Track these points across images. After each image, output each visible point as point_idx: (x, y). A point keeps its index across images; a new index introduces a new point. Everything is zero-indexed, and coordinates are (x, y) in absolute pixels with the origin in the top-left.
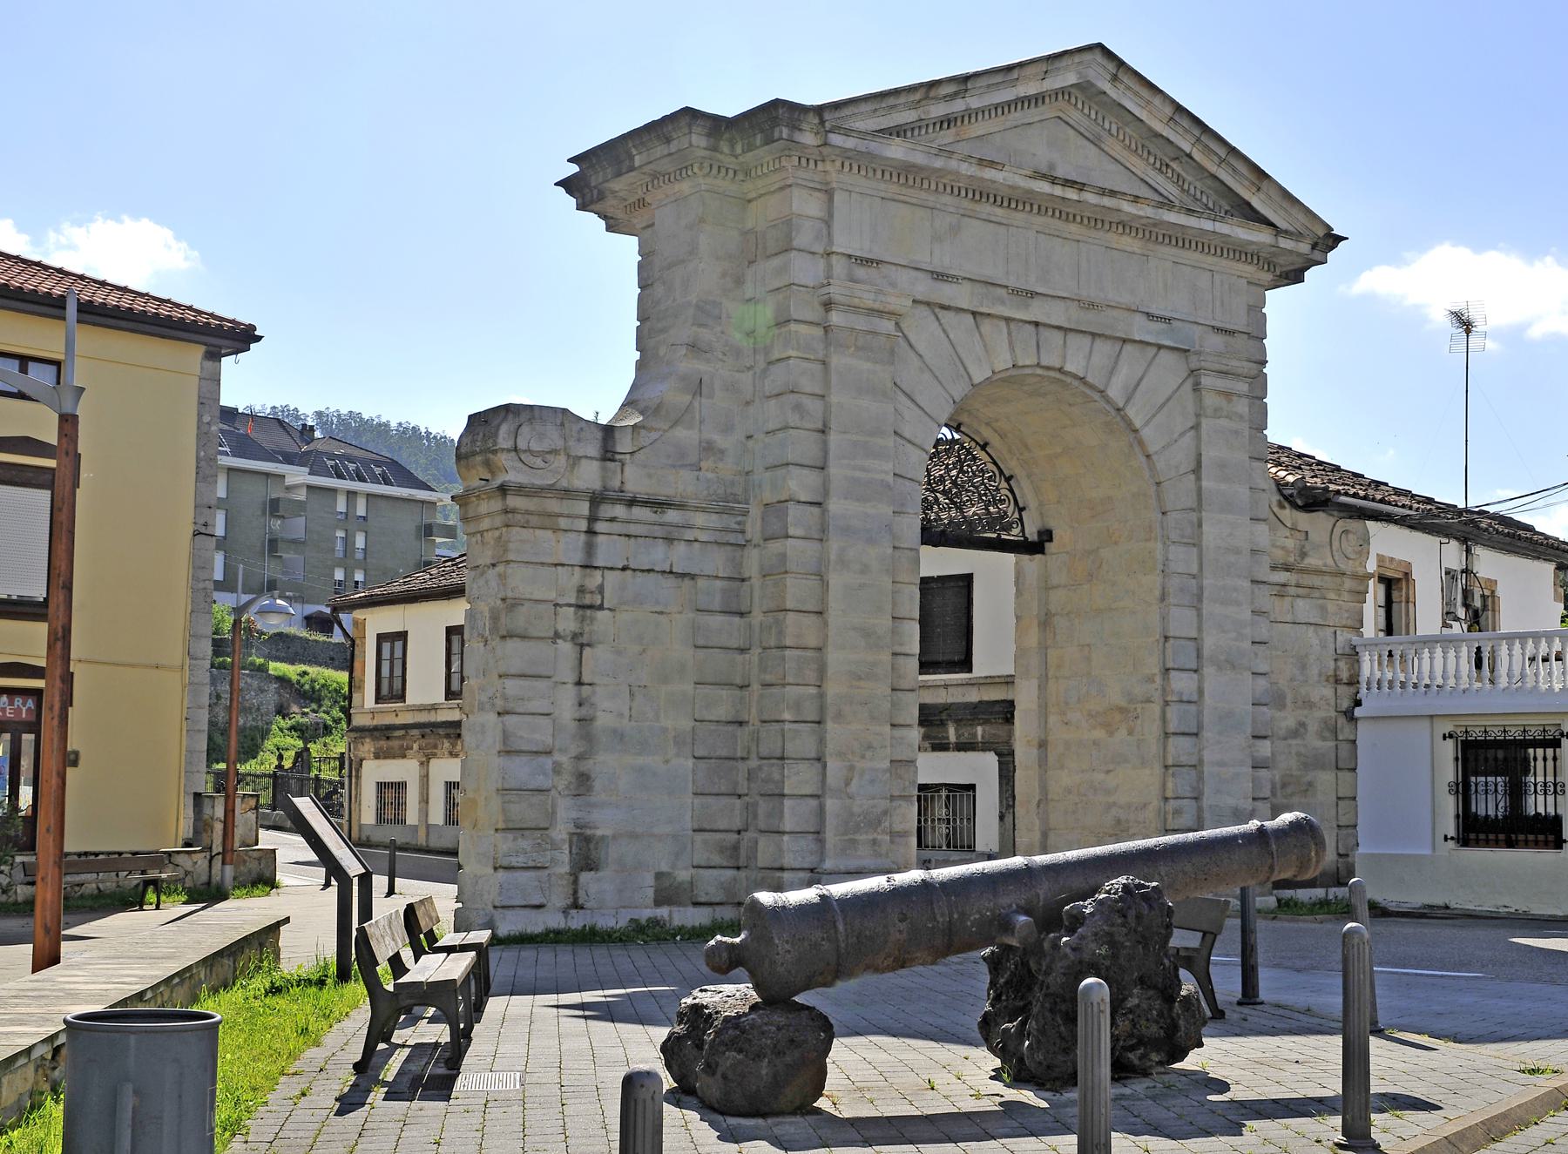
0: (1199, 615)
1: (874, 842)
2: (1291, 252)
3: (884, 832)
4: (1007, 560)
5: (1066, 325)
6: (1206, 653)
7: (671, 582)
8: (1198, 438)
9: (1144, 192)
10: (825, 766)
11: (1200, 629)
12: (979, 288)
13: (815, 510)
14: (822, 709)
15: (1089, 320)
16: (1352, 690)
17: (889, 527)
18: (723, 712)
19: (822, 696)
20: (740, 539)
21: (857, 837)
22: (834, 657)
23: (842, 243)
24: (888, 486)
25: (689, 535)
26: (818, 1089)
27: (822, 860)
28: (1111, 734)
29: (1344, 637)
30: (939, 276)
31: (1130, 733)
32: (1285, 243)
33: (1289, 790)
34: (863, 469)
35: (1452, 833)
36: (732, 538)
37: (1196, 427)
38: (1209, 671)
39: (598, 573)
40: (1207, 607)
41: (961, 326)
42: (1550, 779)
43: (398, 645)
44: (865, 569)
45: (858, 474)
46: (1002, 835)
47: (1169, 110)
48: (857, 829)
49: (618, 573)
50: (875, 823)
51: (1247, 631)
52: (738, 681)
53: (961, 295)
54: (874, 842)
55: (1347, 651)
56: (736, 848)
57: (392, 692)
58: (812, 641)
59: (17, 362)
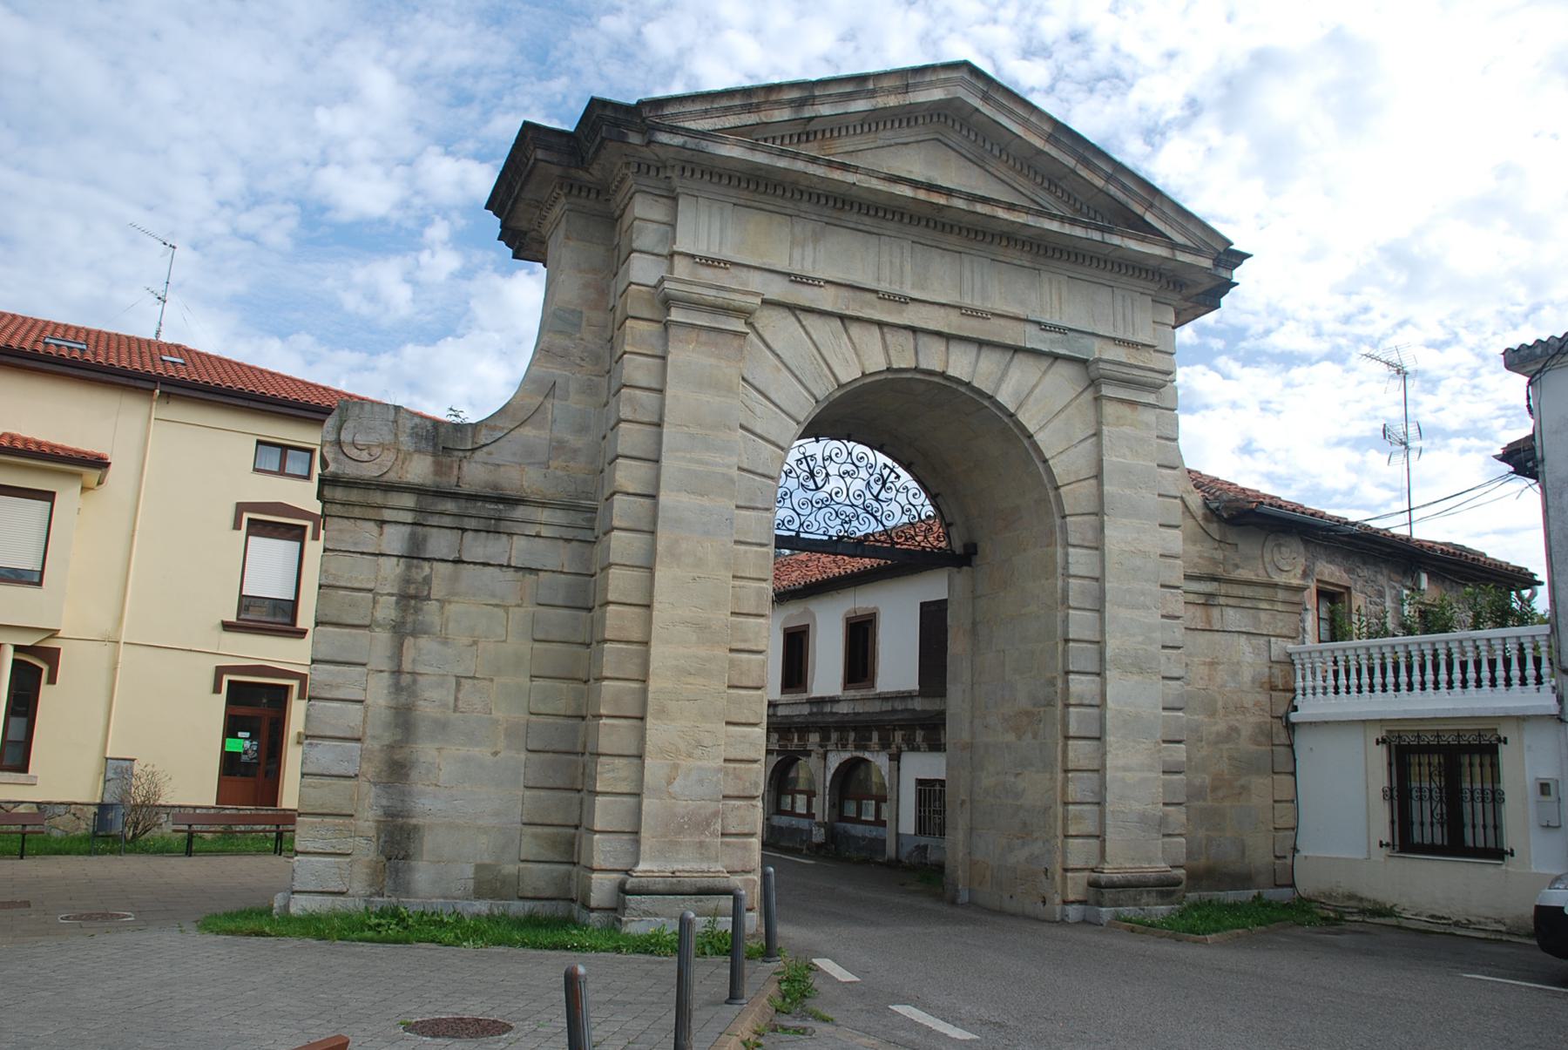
0: (1102, 620)
1: (701, 844)
2: (1101, 190)
3: (713, 834)
5: (946, 330)
6: (1109, 654)
7: (510, 574)
8: (1099, 445)
11: (1103, 632)
12: (844, 293)
13: (647, 501)
14: (644, 704)
16: (1290, 695)
17: (730, 520)
18: (561, 706)
20: (589, 536)
21: (681, 839)
22: (659, 653)
24: (732, 481)
25: (532, 530)
27: (637, 863)
29: (1279, 647)
31: (1035, 737)
32: (1182, 257)
33: (1220, 794)
35: (1386, 839)
36: (581, 534)
37: (1097, 434)
38: (1110, 674)
39: (426, 565)
42: (1488, 786)
45: (694, 467)
47: (1047, 128)
48: (680, 830)
49: (450, 565)
51: (1157, 635)
53: (826, 299)
54: (701, 844)
55: (1282, 658)
58: (636, 635)
59: (279, 450)
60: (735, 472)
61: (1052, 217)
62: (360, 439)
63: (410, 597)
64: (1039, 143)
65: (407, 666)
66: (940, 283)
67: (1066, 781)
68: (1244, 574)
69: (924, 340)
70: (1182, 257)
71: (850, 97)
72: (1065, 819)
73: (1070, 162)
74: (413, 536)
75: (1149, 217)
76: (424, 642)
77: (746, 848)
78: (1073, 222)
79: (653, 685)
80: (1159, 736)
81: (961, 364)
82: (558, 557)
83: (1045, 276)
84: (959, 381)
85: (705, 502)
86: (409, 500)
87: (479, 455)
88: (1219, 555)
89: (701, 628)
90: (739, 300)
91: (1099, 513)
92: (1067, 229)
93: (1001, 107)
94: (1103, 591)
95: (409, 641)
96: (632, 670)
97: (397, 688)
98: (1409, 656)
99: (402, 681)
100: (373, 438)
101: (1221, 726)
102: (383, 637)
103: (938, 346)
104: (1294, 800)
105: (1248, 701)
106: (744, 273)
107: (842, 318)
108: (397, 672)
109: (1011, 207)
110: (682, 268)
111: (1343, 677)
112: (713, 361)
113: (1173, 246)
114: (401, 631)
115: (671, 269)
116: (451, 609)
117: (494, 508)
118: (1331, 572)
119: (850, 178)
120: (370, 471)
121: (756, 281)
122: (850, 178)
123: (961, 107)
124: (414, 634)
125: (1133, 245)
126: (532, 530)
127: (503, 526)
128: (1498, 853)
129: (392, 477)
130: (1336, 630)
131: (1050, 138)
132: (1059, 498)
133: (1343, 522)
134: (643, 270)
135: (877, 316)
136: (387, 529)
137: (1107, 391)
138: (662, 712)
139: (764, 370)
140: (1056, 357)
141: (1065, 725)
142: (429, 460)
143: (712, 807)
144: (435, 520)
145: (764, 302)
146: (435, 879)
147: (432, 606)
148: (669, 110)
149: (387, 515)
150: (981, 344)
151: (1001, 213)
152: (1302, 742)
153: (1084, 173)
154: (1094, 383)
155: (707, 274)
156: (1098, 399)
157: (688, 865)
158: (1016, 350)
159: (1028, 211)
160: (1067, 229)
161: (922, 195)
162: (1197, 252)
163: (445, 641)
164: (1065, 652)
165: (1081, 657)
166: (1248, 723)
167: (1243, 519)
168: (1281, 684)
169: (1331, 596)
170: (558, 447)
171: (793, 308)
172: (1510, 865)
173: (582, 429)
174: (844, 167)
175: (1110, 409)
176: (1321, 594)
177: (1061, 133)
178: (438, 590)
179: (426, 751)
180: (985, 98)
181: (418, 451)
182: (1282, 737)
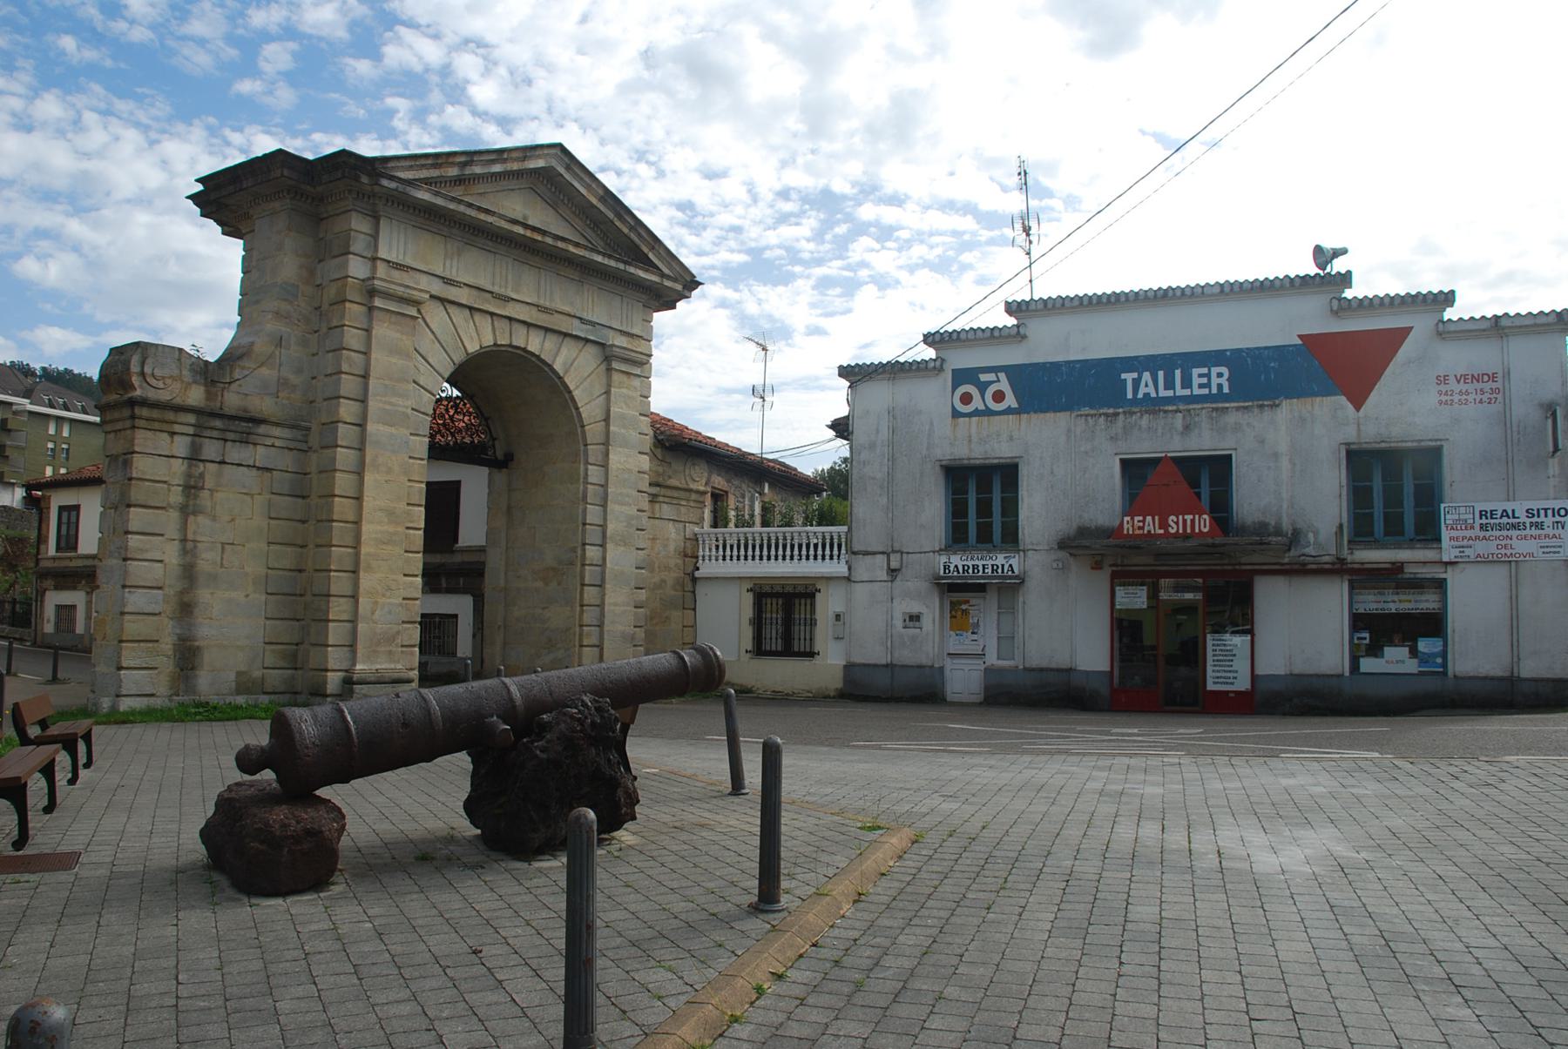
0: (605, 512)
4: (482, 473)
7: (254, 472)
8: (608, 400)
9: (582, 241)
10: (357, 602)
11: (605, 519)
12: (475, 292)
15: (542, 319)
19: (357, 555)
20: (304, 447)
22: (366, 528)
23: (382, 254)
24: (407, 416)
25: (269, 442)
26: (456, 540)
28: (546, 584)
30: (448, 282)
32: (667, 283)
34: (390, 403)
37: (608, 393)
38: (609, 546)
40: (610, 506)
41: (460, 316)
43: (74, 513)
44: (389, 471)
46: (474, 647)
47: (601, 192)
50: (391, 639)
52: (299, 542)
53: (463, 296)
56: (294, 656)
57: (69, 541)
60: (409, 411)
61: (599, 253)
62: (158, 372)
63: (192, 487)
64: (594, 201)
65: (190, 536)
66: (529, 290)
67: (582, 612)
68: (674, 482)
69: (515, 325)
70: (667, 283)
71: (493, 162)
72: (581, 635)
73: (611, 215)
74: (193, 444)
75: (651, 256)
76: (200, 518)
77: (412, 654)
78: (610, 257)
79: (364, 550)
80: (633, 584)
81: (535, 343)
82: (286, 461)
83: (586, 287)
84: (533, 354)
85: (393, 430)
86: (191, 419)
87: (234, 386)
88: (660, 470)
89: (391, 513)
90: (416, 295)
91: (606, 443)
92: (606, 261)
93: (576, 175)
94: (606, 494)
95: (191, 519)
96: (349, 541)
97: (184, 552)
98: (747, 540)
99: (188, 547)
100: (166, 372)
101: (656, 579)
102: (174, 515)
103: (522, 330)
104: (694, 626)
105: (672, 563)
106: (418, 275)
107: (471, 309)
108: (184, 540)
109: (577, 245)
110: (382, 270)
111: (725, 550)
112: (398, 335)
113: (663, 275)
114: (186, 511)
115: (374, 269)
116: (218, 495)
117: (245, 426)
118: (719, 481)
119: (490, 219)
120: (164, 396)
121: (424, 282)
122: (490, 219)
123: (554, 175)
124: (195, 513)
125: (642, 274)
126: (269, 442)
127: (252, 438)
128: (811, 654)
129: (178, 401)
130: (719, 520)
131: (601, 199)
132: (584, 433)
133: (719, 445)
134: (357, 268)
135: (492, 309)
136: (176, 438)
137: (615, 365)
138: (369, 568)
139: (426, 344)
140: (587, 341)
141: (582, 578)
142: (202, 389)
143: (396, 628)
144: (208, 433)
145: (432, 296)
146: (211, 682)
147: (205, 494)
148: (391, 164)
149: (177, 428)
150: (547, 330)
151: (571, 248)
152: (701, 590)
153: (618, 223)
154: (607, 359)
155: (396, 274)
156: (609, 370)
157: (383, 665)
158: (566, 335)
159: (586, 248)
160: (606, 261)
161: (528, 233)
162: (675, 280)
163: (214, 519)
164: (584, 531)
165: (593, 535)
166: (671, 577)
167: (678, 446)
168: (690, 554)
169: (718, 497)
170: (283, 383)
171: (444, 301)
172: (817, 660)
173: (299, 371)
174: (487, 211)
175: (616, 377)
176: (713, 495)
177: (609, 197)
178: (209, 482)
179: (204, 595)
180: (568, 168)
181: (195, 382)
182: (689, 587)
